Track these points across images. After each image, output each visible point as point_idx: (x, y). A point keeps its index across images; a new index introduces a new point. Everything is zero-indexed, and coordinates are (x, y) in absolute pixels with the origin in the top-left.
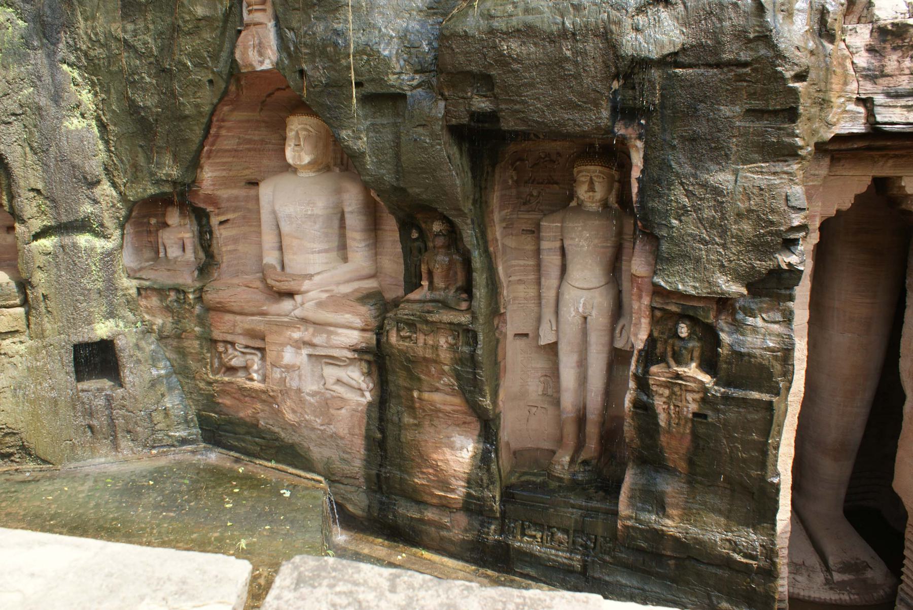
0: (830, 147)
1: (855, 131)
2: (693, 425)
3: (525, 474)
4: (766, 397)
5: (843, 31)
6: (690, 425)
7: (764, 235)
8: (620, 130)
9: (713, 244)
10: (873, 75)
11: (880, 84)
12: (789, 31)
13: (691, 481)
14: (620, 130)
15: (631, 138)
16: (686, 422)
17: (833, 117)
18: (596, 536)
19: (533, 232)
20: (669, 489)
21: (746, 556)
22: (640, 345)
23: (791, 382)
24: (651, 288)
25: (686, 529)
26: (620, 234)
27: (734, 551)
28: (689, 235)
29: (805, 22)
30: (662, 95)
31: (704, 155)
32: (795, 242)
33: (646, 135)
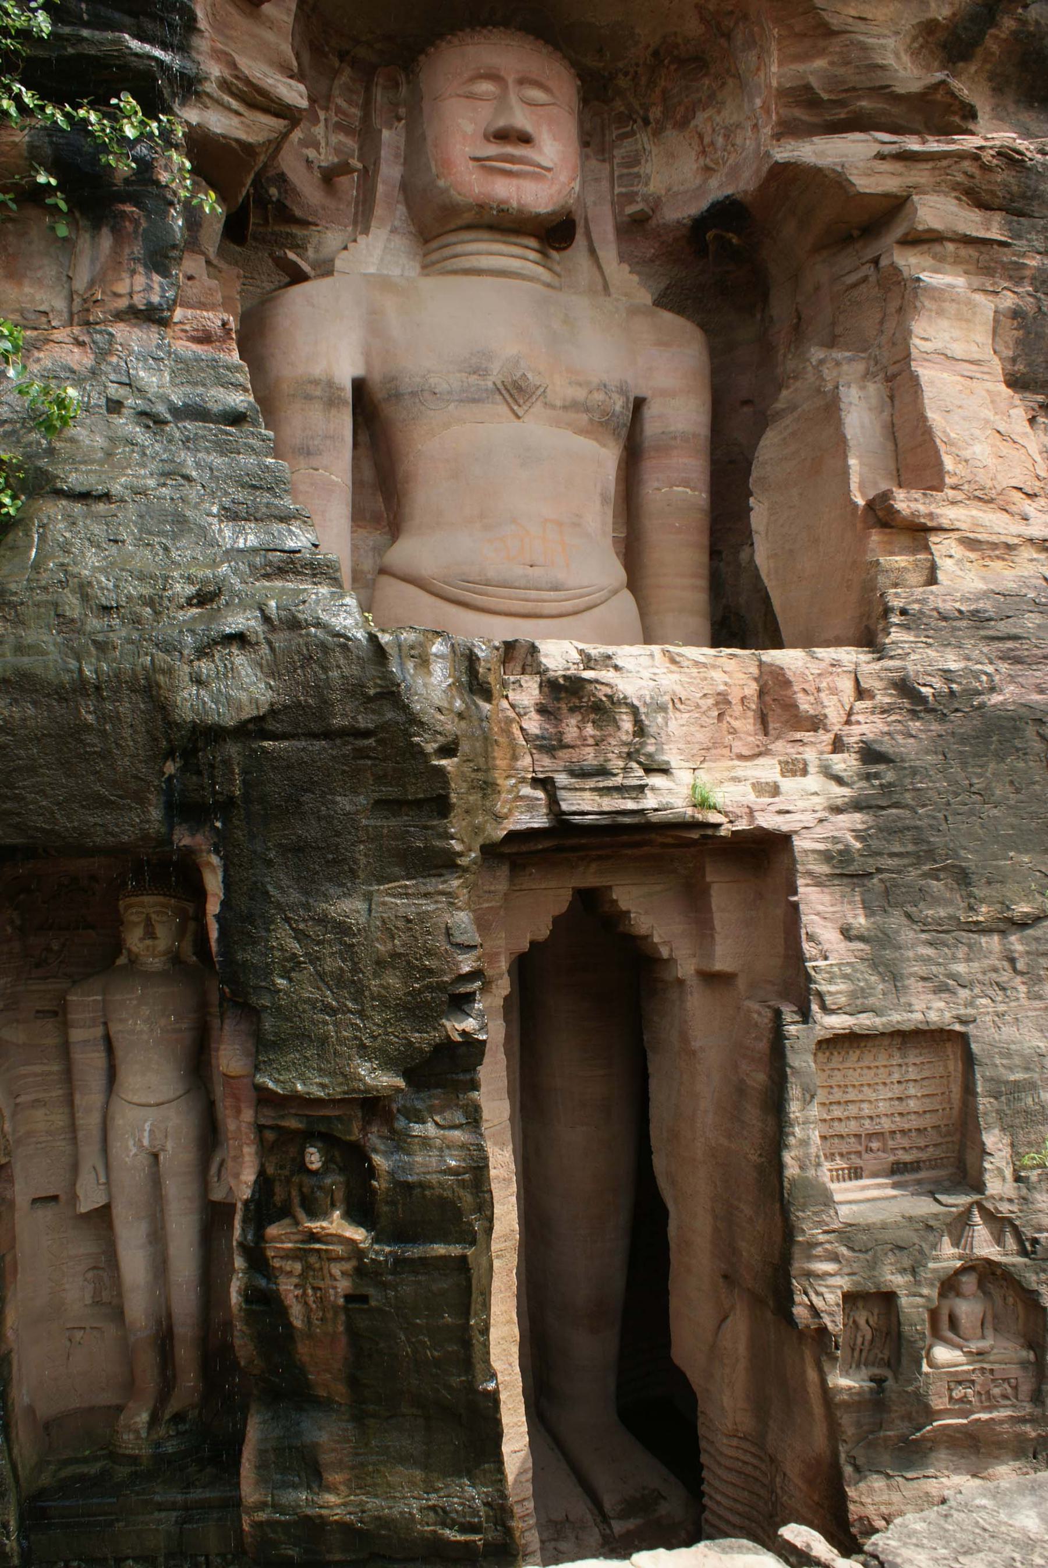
0: (507, 850)
1: (536, 826)
2: (348, 1317)
3: (66, 1463)
4: (455, 1250)
5: (504, 684)
6: (342, 1317)
7: (420, 992)
8: (183, 838)
9: (344, 1013)
10: (550, 745)
11: (560, 759)
12: (425, 685)
13: (359, 1418)
14: (183, 838)
15: (201, 851)
16: (336, 1313)
17: (503, 807)
18: (207, 1557)
19: (55, 1013)
20: (323, 1438)
21: (464, 1529)
22: (246, 1193)
23: (491, 1220)
24: (252, 1094)
25: (361, 1504)
26: (202, 1007)
27: (444, 1525)
28: (305, 1002)
29: (446, 672)
30: (244, 782)
31: (317, 873)
32: (469, 998)
33: (222, 844)
